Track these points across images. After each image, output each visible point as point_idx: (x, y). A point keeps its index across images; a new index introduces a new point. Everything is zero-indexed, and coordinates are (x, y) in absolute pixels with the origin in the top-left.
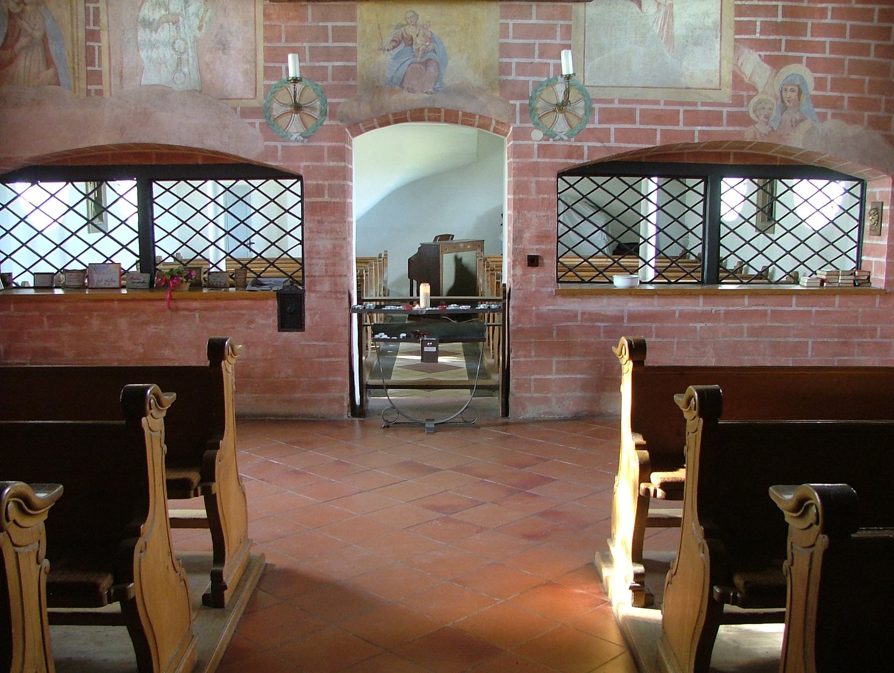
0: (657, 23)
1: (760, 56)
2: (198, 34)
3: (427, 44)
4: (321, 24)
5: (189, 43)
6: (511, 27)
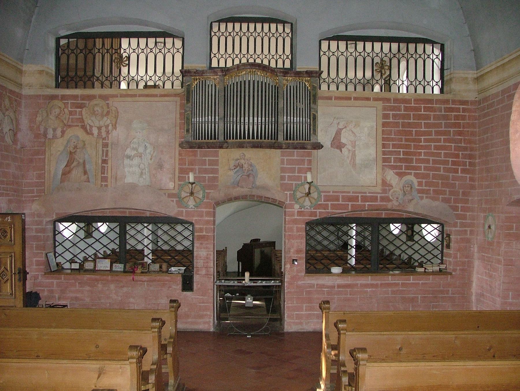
0: (349, 159)
1: (393, 172)
2: (150, 162)
3: (249, 167)
4: (204, 158)
5: (146, 166)
6: (285, 160)
